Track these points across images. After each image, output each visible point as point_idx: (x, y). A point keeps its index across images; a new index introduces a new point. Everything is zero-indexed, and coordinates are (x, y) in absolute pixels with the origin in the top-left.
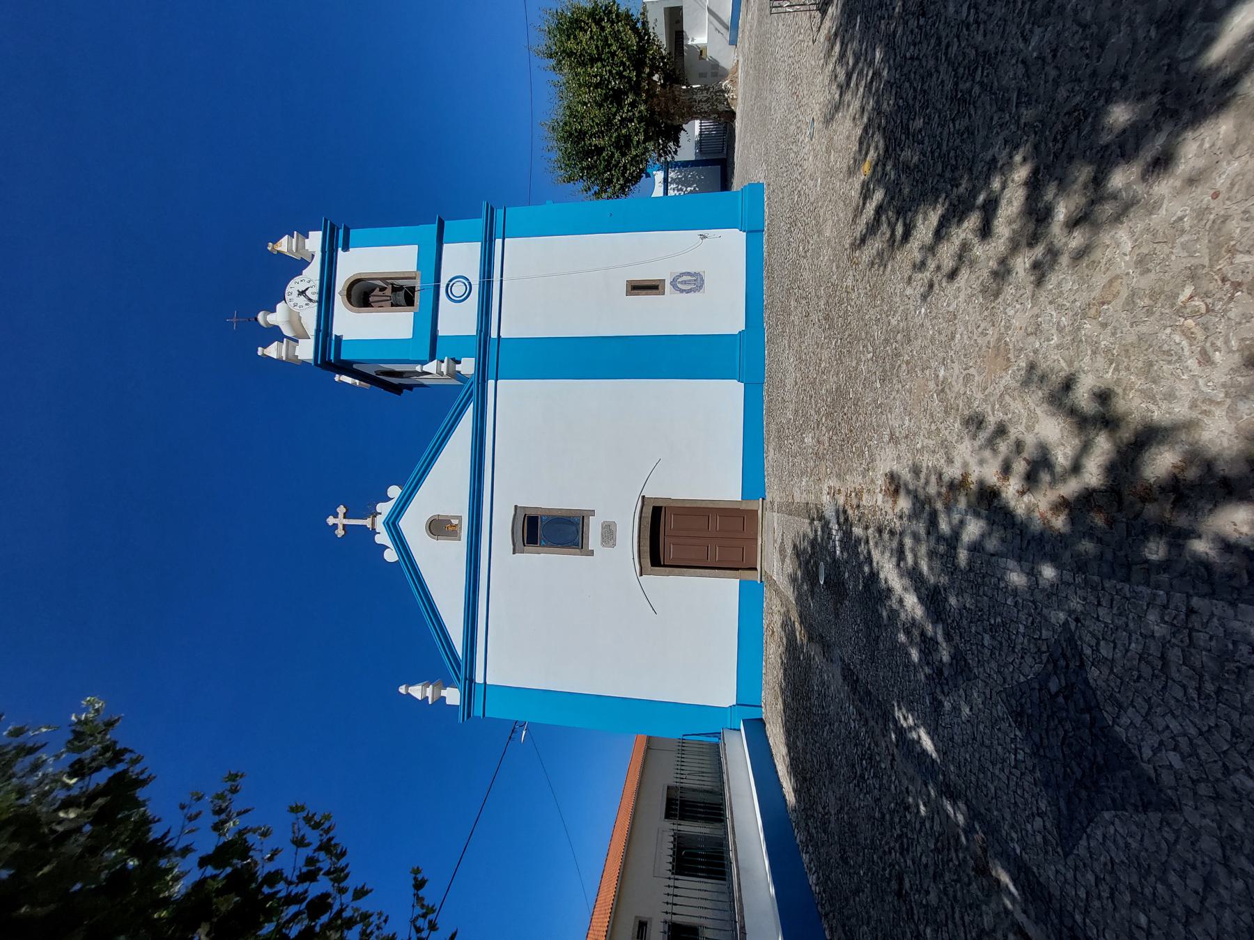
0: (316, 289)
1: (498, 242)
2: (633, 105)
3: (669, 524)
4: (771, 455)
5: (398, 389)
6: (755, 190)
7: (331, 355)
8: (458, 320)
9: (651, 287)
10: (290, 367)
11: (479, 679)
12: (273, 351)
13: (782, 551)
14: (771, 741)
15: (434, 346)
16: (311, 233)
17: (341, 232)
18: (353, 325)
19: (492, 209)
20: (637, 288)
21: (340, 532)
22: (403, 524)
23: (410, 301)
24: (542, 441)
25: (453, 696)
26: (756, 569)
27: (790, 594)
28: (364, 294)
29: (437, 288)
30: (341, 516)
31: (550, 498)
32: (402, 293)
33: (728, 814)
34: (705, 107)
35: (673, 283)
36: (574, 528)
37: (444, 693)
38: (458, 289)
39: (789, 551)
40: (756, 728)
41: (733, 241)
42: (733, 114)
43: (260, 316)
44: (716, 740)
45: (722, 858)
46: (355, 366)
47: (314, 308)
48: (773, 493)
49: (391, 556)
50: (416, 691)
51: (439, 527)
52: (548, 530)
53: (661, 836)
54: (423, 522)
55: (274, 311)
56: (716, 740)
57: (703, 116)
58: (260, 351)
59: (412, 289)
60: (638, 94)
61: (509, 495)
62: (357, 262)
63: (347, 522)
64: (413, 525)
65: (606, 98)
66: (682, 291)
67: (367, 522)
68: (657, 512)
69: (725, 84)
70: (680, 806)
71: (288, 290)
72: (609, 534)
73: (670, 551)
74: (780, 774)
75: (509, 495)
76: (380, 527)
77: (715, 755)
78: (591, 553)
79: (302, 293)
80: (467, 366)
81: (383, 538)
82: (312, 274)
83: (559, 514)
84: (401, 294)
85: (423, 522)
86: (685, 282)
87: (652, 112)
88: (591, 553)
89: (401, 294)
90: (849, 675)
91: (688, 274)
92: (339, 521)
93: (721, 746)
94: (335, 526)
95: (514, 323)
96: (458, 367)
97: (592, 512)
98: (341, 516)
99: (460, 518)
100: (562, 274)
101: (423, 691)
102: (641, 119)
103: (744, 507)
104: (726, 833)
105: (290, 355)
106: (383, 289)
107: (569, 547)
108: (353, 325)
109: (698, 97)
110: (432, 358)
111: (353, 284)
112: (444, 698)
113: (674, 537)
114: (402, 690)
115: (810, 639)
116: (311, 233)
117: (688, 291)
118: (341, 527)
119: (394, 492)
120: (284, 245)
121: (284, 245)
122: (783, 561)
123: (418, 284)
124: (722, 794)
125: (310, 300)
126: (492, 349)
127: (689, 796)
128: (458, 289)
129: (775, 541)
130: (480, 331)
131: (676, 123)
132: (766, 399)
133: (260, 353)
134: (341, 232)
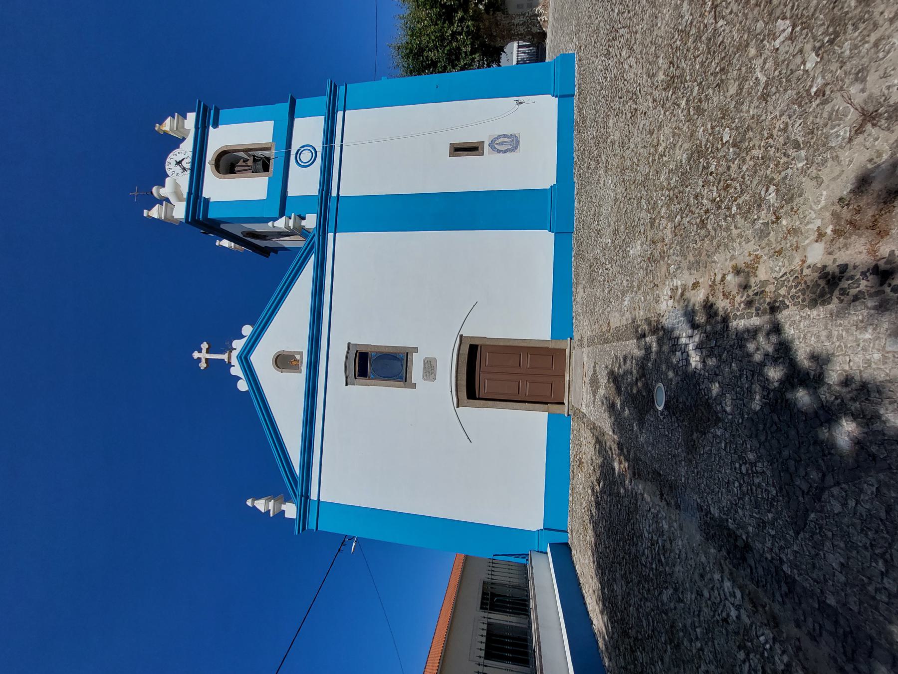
0: (190, 160)
1: (340, 114)
2: (462, 20)
3: (484, 362)
4: (580, 295)
5: (265, 252)
6: (566, 60)
7: (203, 220)
8: (304, 182)
9: (472, 149)
10: (165, 226)
11: (314, 496)
12: (155, 212)
13: (594, 384)
14: (578, 568)
15: (283, 204)
16: (188, 114)
17: (212, 112)
18: (219, 189)
19: (335, 87)
20: (459, 150)
21: (203, 365)
22: (254, 358)
23: (266, 168)
24: (374, 285)
25: (291, 510)
26: (563, 404)
27: (606, 425)
28: (229, 163)
29: (288, 154)
30: (204, 351)
31: (378, 337)
32: (260, 163)
33: (532, 605)
34: (522, 30)
35: (491, 145)
36: (400, 363)
37: (284, 507)
38: (306, 156)
39: (603, 380)
40: (562, 553)
41: (546, 106)
42: (544, 35)
43: (154, 190)
44: (523, 561)
45: (526, 647)
46: (222, 226)
47: (187, 175)
48: (583, 328)
49: (243, 386)
50: (260, 505)
51: (284, 361)
52: (376, 365)
53: (476, 623)
54: (269, 357)
55: (163, 185)
56: (523, 561)
57: (520, 37)
58: (145, 213)
59: (269, 159)
60: (466, 11)
61: (346, 332)
62: (221, 137)
63: (209, 356)
64: (261, 359)
65: (439, 16)
66: (499, 151)
67: (225, 357)
68: (473, 350)
69: (539, 9)
70: (492, 599)
71: (168, 161)
72: (430, 369)
73: (484, 385)
74: (590, 607)
75: (346, 332)
76: (234, 361)
77: (524, 572)
78: (414, 386)
79: (179, 163)
80: (311, 222)
81: (236, 370)
82: (187, 147)
83: (386, 350)
84: (259, 162)
85: (269, 357)
86: (502, 144)
87: (478, 29)
88: (414, 386)
89: (259, 162)
90: (716, 531)
91: (505, 136)
92: (202, 355)
93: (529, 568)
94: (199, 359)
95: (352, 183)
96: (303, 223)
97: (415, 350)
98: (204, 351)
99: (301, 353)
100: (395, 140)
101: (266, 505)
102: (468, 33)
103: (553, 346)
104: (530, 623)
105: (168, 216)
106: (246, 161)
107: (395, 380)
108: (219, 189)
109: (516, 21)
110: (282, 214)
111: (222, 155)
112: (284, 512)
113: (488, 373)
114: (249, 503)
115: (637, 474)
116: (188, 114)
117: (505, 151)
118: (203, 360)
119: (247, 330)
120: (168, 125)
121: (168, 125)
122: (595, 393)
123: (272, 153)
124: (528, 591)
125: (184, 169)
126: (332, 206)
127: (498, 590)
128: (306, 156)
129: (584, 375)
130: (322, 190)
131: (498, 44)
132: (574, 247)
133: (145, 215)
134: (212, 112)
